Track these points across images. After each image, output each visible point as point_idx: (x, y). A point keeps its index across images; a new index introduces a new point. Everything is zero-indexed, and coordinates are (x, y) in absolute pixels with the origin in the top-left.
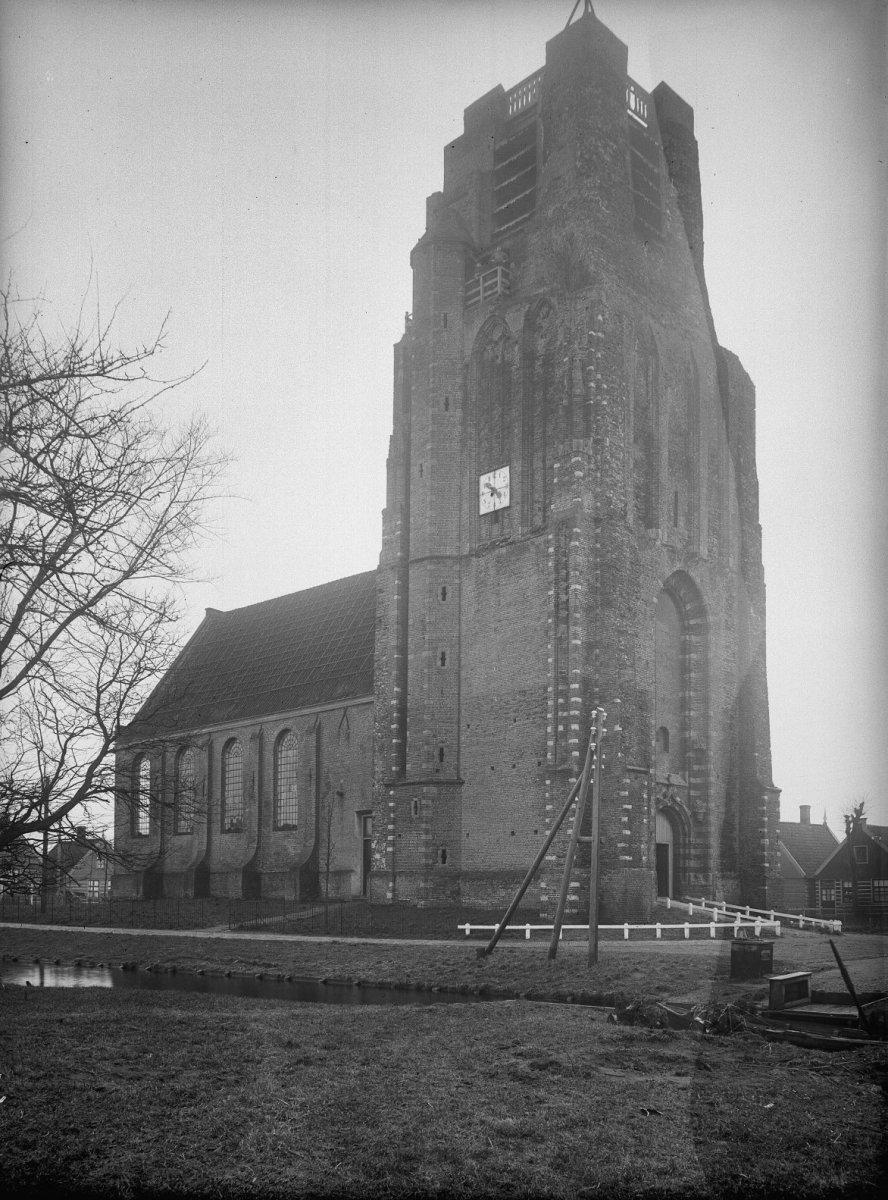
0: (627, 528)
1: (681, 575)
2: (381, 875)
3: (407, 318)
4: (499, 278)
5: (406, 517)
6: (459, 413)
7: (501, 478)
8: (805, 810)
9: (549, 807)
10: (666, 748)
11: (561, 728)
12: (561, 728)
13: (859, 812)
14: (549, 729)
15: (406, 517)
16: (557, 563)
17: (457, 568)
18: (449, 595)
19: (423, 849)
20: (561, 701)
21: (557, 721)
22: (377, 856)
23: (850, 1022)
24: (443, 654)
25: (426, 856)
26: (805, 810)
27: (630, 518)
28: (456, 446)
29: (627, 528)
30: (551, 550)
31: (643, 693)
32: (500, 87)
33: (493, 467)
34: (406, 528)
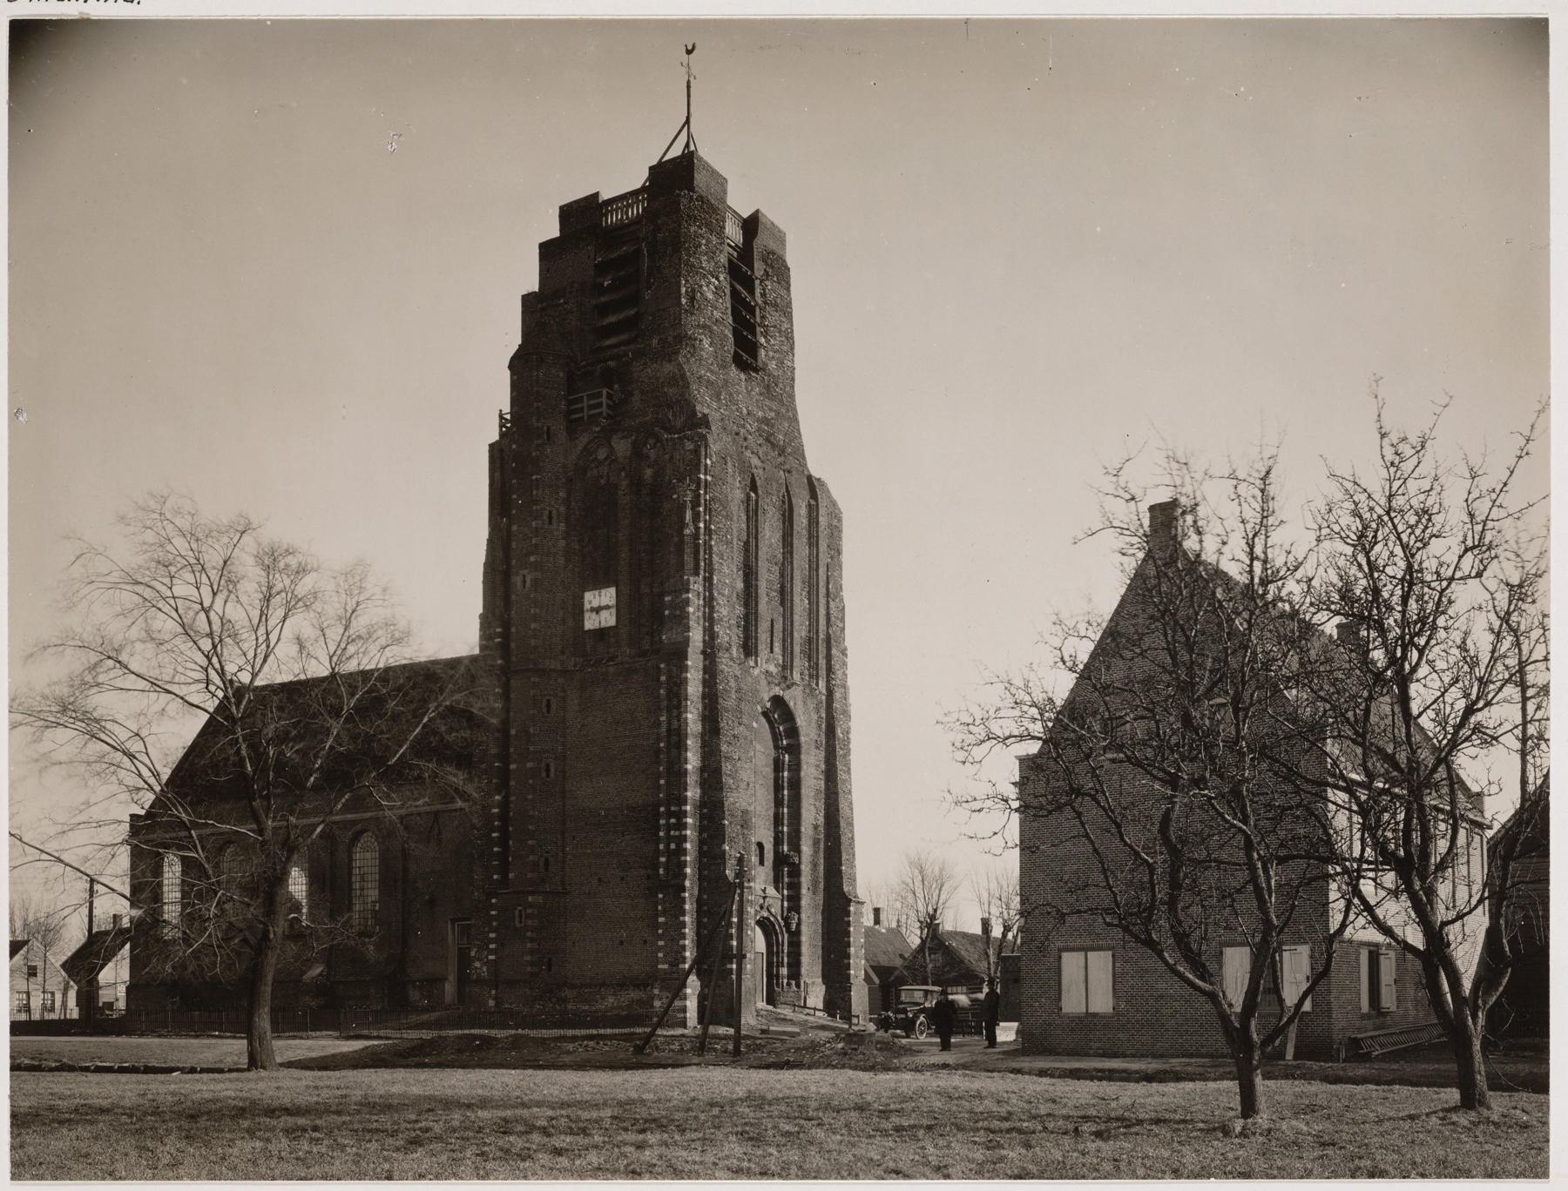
0: (732, 659)
1: (778, 701)
2: (480, 981)
3: (501, 417)
4: (604, 400)
5: (506, 625)
6: (562, 527)
7: (608, 596)
8: (901, 956)
9: (661, 920)
10: (762, 863)
11: (673, 846)
12: (673, 846)
13: (933, 917)
14: (661, 847)
15: (506, 625)
16: (669, 691)
17: (561, 680)
18: (554, 707)
19: (528, 958)
20: (673, 821)
21: (669, 839)
22: (477, 964)
23: (794, 1169)
24: (548, 765)
25: (531, 964)
26: (901, 956)
27: (734, 651)
28: (561, 561)
29: (732, 659)
30: (663, 678)
31: (745, 812)
32: (597, 194)
33: (598, 585)
34: (506, 636)
